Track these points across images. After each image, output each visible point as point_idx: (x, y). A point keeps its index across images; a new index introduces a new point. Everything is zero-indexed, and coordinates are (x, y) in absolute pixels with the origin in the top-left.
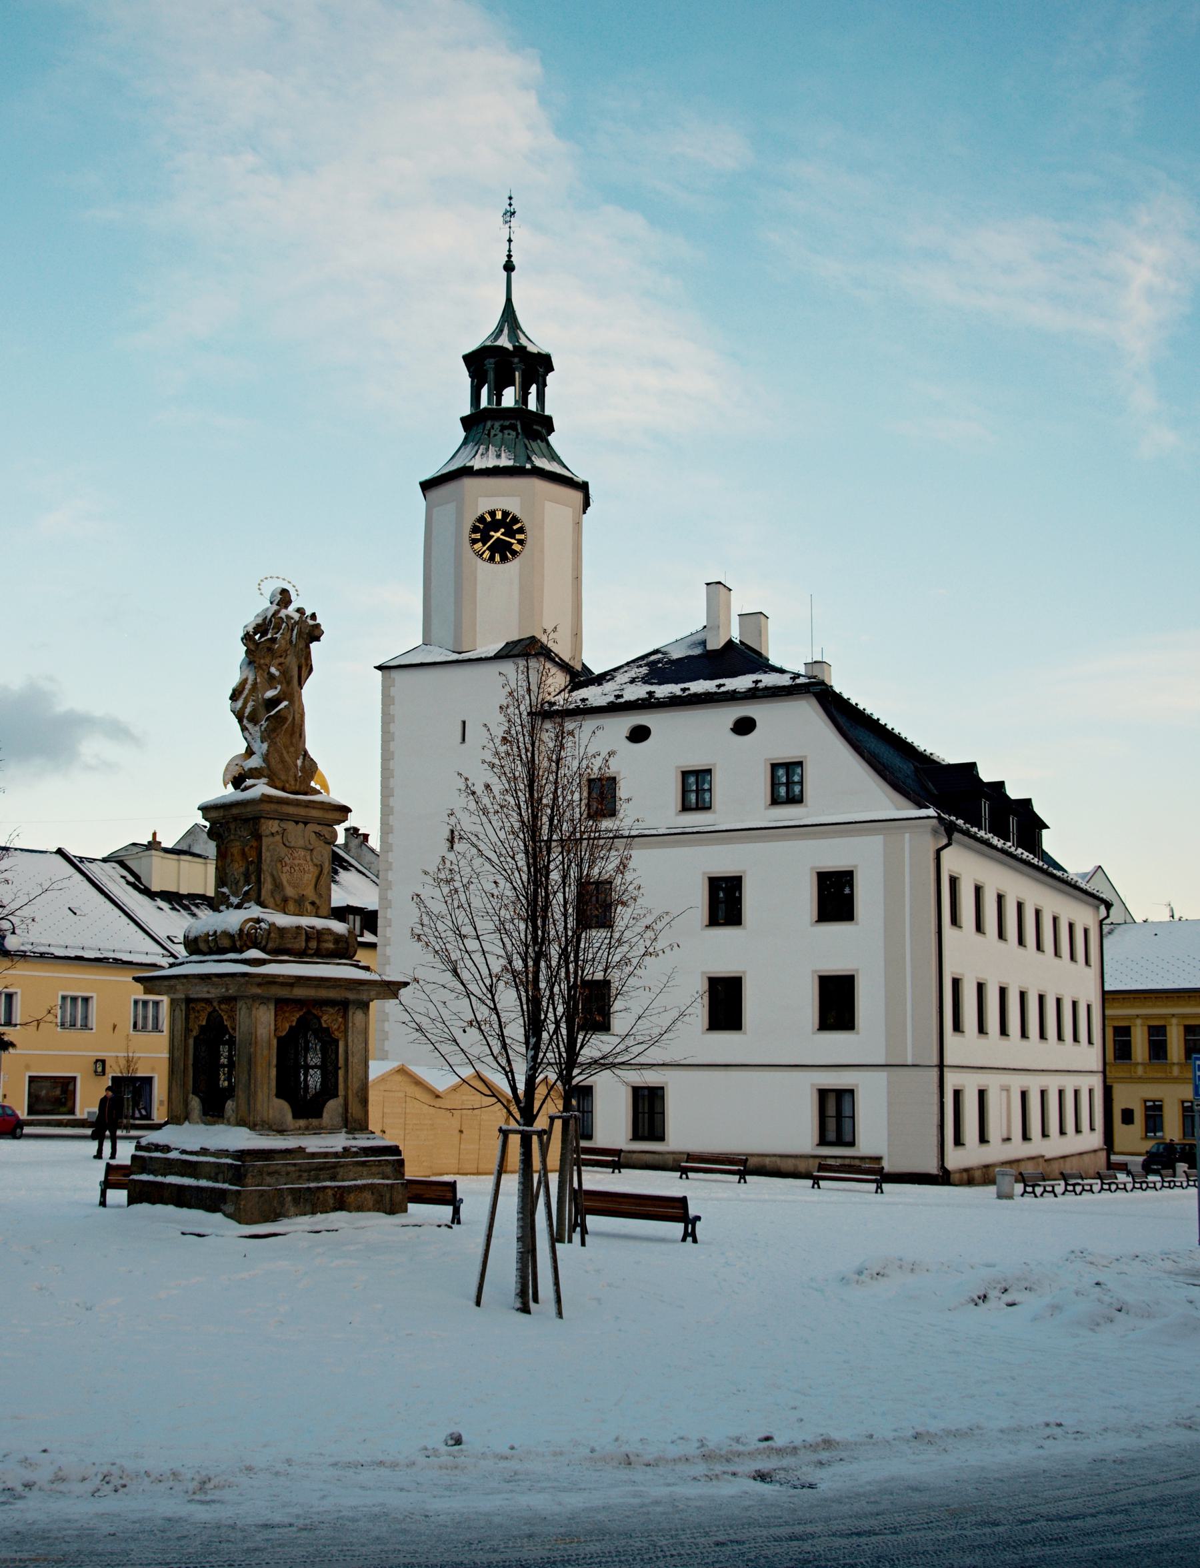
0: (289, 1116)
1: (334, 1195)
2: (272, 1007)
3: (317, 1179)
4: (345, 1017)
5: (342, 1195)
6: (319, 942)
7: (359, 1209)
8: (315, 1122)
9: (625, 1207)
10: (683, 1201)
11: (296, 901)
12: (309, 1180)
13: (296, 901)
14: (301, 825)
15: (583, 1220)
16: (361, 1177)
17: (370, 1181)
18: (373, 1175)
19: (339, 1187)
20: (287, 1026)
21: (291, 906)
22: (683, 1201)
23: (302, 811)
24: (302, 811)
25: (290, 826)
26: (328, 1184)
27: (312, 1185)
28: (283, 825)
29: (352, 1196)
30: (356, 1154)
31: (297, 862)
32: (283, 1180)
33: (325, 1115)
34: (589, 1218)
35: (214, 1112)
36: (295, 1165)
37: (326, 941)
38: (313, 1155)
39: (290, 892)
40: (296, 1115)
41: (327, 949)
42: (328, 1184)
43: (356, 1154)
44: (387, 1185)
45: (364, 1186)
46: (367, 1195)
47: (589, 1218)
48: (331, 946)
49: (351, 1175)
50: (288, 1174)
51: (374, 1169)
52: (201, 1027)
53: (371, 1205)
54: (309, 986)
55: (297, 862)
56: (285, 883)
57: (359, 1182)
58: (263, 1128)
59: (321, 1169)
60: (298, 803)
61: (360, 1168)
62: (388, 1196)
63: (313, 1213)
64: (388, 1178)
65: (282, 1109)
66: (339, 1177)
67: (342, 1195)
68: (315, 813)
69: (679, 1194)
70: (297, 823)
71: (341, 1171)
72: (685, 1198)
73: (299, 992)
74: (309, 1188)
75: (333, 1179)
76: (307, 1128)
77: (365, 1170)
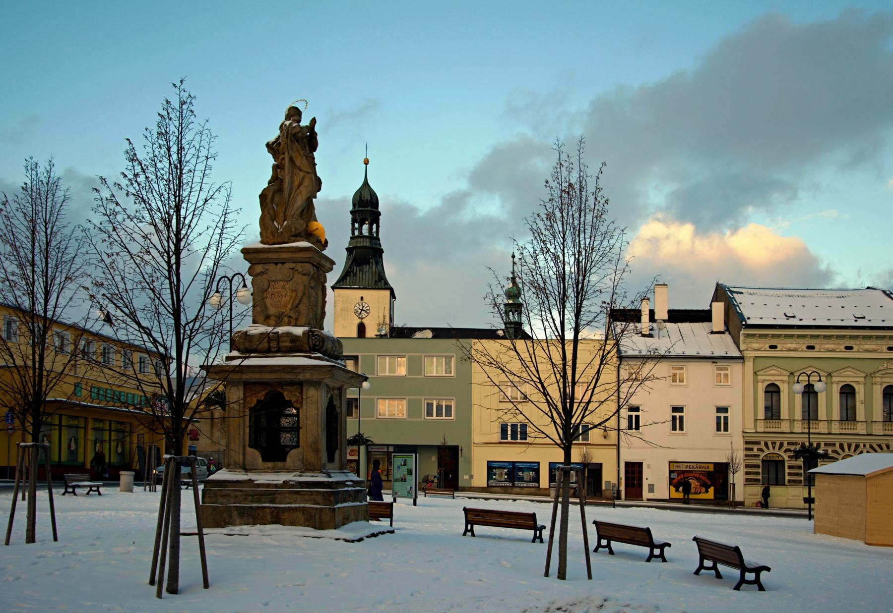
0: (260, 460)
1: (272, 513)
2: (241, 388)
3: (259, 501)
4: (301, 393)
5: (278, 513)
6: (278, 342)
7: (292, 523)
8: (280, 464)
9: (504, 521)
10: (533, 516)
11: (276, 316)
12: (252, 502)
13: (276, 316)
14: (280, 265)
15: (472, 527)
16: (295, 502)
17: (302, 505)
18: (306, 502)
19: (275, 508)
20: (255, 400)
21: (272, 322)
22: (533, 516)
23: (275, 256)
24: (275, 256)
25: (272, 267)
26: (267, 505)
27: (254, 505)
28: (266, 267)
29: (286, 514)
30: (293, 486)
31: (276, 290)
32: (233, 501)
33: (288, 459)
34: (475, 527)
35: (274, 454)
36: (241, 491)
37: (284, 341)
38: (259, 485)
39: (272, 311)
40: (265, 459)
41: (286, 347)
42: (267, 505)
43: (293, 486)
44: (316, 509)
45: (296, 508)
46: (299, 515)
47: (475, 527)
48: (288, 344)
49: (287, 500)
50: (236, 496)
51: (306, 497)
52: (258, 401)
53: (302, 522)
54: (254, 372)
55: (276, 290)
56: (268, 305)
57: (293, 505)
58: (235, 467)
59: (262, 495)
60: (277, 251)
61: (295, 496)
62: (317, 516)
63: (255, 524)
64: (319, 504)
65: (254, 455)
66: (277, 500)
67: (278, 513)
68: (285, 255)
69: (531, 512)
70: (276, 264)
71: (279, 497)
72: (534, 514)
73: (267, 377)
74: (251, 507)
75: (271, 502)
76: (274, 468)
77: (299, 498)
